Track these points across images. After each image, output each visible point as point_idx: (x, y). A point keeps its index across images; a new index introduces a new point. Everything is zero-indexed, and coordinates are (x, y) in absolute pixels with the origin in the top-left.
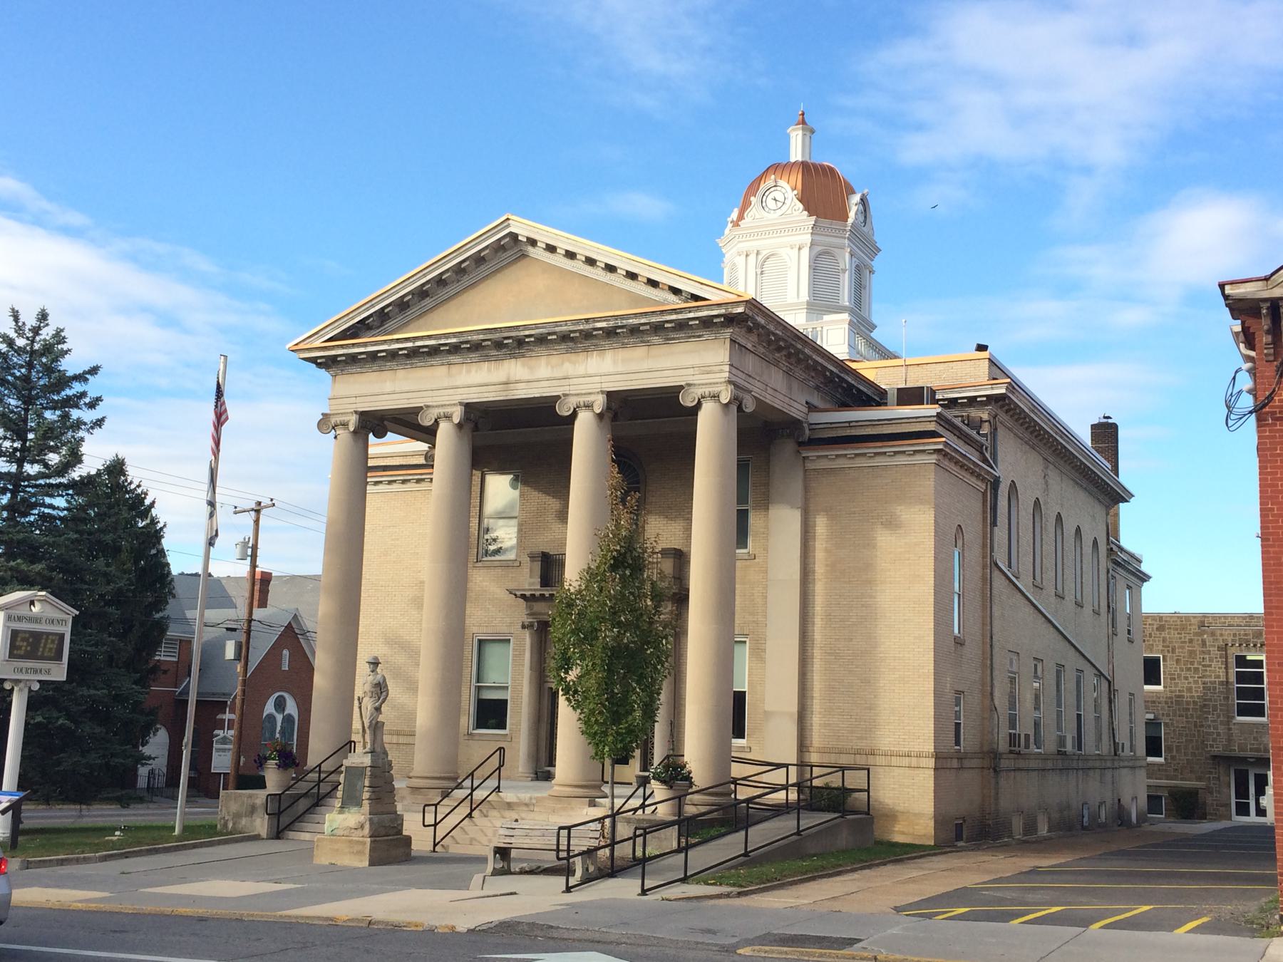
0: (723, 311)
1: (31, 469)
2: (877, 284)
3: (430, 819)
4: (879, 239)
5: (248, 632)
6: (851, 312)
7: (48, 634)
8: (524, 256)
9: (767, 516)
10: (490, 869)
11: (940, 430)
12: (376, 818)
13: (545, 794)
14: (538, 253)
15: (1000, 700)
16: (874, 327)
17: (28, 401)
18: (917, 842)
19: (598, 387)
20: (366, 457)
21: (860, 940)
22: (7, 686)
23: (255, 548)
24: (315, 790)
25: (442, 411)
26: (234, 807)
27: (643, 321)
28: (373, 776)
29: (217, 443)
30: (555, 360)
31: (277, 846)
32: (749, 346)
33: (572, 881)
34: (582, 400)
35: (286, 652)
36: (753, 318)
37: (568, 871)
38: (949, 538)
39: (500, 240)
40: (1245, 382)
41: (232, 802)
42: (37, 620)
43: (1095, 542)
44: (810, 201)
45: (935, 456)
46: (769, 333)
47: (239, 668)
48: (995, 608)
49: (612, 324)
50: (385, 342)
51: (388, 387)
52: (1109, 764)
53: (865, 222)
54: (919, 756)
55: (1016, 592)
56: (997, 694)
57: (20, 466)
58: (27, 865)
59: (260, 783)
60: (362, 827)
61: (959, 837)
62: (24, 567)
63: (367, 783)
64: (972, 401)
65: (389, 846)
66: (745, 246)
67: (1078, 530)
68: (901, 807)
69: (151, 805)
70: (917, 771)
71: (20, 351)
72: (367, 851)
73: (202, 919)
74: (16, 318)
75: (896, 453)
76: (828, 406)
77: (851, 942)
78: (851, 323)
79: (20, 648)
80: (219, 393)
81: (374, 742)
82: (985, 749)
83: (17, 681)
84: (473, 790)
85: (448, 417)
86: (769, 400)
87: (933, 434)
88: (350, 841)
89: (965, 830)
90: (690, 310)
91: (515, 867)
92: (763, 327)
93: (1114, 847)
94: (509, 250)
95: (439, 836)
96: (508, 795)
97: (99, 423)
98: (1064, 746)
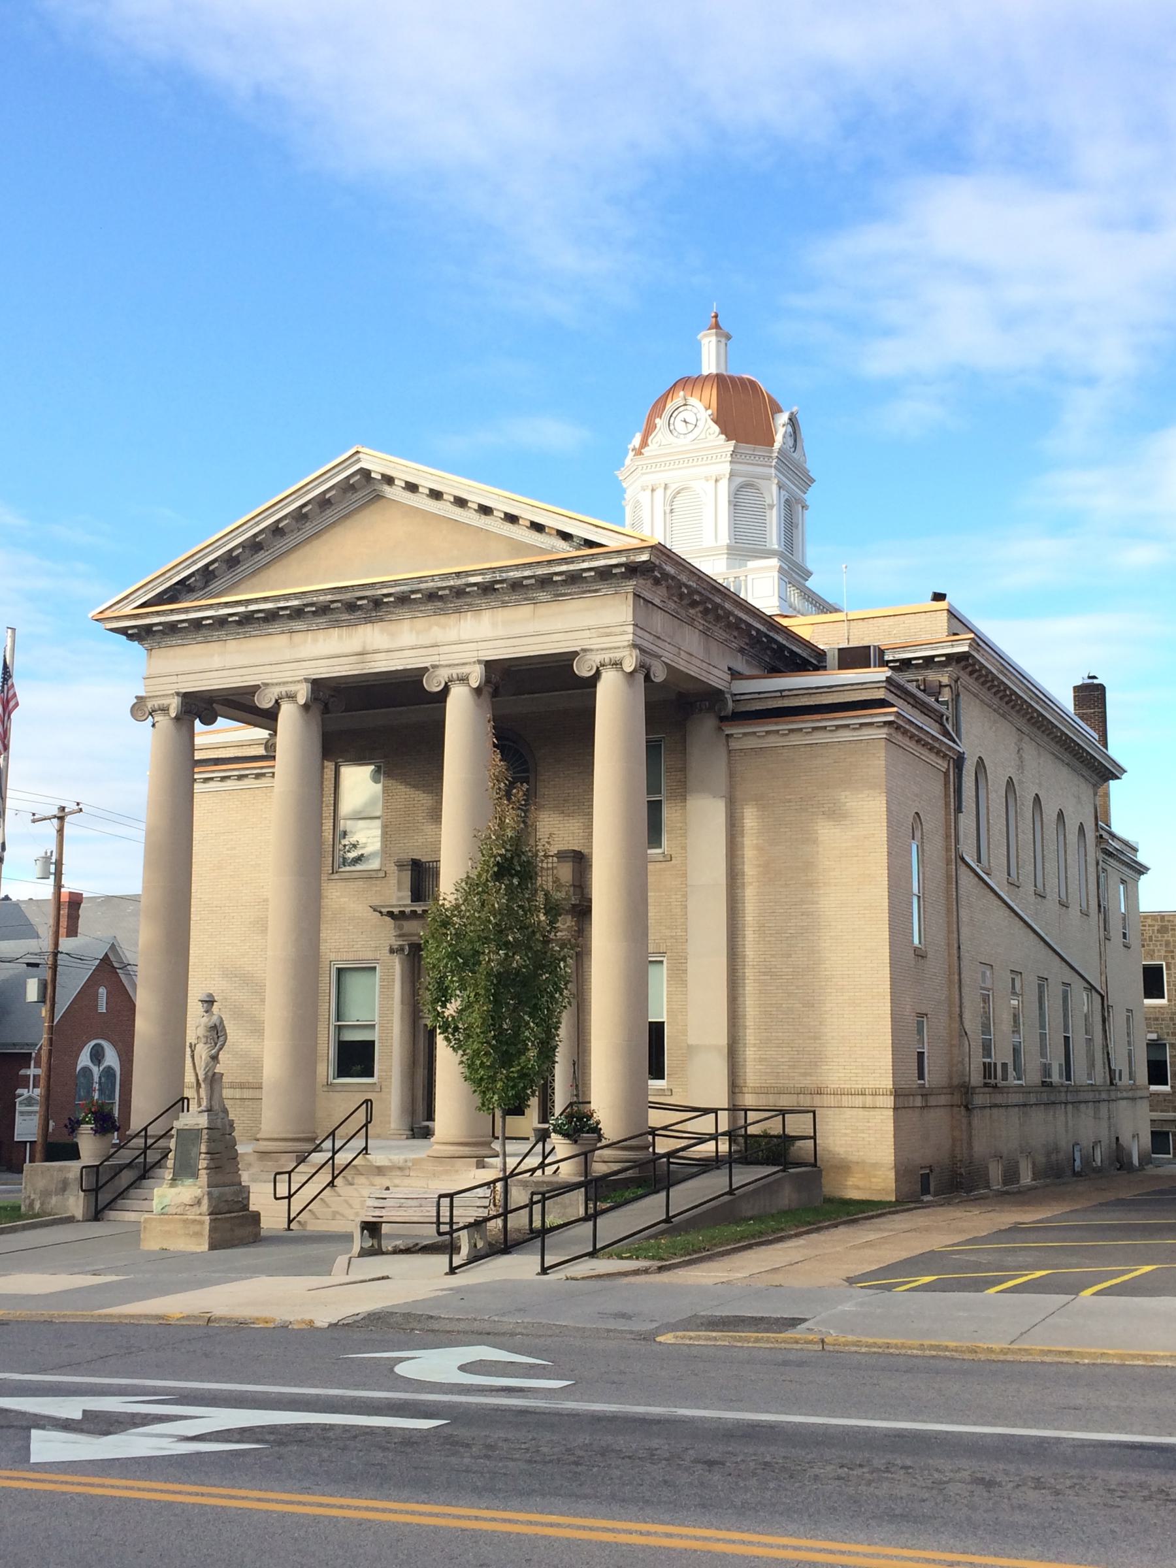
0: (623, 560)
2: (811, 521)
3: (283, 1190)
4: (813, 466)
5: (55, 968)
8: (379, 497)
10: (356, 1249)
11: (891, 698)
15: (972, 1024)
16: (809, 574)
18: (875, 1197)
19: (472, 656)
21: (805, 1320)
23: (59, 864)
24: (141, 1159)
26: (41, 1183)
27: (527, 573)
28: (210, 1140)
30: (420, 623)
31: (96, 1229)
32: (657, 601)
33: (457, 1260)
34: (455, 672)
35: (102, 991)
36: (660, 568)
37: (452, 1248)
38: (905, 828)
39: (348, 478)
43: (1081, 828)
44: (727, 422)
45: (885, 730)
46: (680, 584)
48: (962, 913)
49: (488, 578)
50: (211, 606)
51: (217, 662)
52: (1104, 1096)
53: (795, 446)
56: (967, 1016)
59: (73, 1153)
60: (199, 1202)
61: (925, 1190)
63: (203, 1149)
64: (929, 661)
65: (234, 1224)
67: (1061, 815)
68: (854, 1158)
76: (755, 672)
77: (794, 1322)
81: (210, 1099)
82: (956, 1082)
84: (334, 1153)
85: (291, 697)
86: (681, 665)
87: (882, 703)
88: (185, 1221)
89: (936, 1181)
90: (583, 558)
91: (387, 1245)
92: (673, 578)
93: (1111, 1196)
94: (360, 491)
96: (377, 1158)
98: (1050, 1076)
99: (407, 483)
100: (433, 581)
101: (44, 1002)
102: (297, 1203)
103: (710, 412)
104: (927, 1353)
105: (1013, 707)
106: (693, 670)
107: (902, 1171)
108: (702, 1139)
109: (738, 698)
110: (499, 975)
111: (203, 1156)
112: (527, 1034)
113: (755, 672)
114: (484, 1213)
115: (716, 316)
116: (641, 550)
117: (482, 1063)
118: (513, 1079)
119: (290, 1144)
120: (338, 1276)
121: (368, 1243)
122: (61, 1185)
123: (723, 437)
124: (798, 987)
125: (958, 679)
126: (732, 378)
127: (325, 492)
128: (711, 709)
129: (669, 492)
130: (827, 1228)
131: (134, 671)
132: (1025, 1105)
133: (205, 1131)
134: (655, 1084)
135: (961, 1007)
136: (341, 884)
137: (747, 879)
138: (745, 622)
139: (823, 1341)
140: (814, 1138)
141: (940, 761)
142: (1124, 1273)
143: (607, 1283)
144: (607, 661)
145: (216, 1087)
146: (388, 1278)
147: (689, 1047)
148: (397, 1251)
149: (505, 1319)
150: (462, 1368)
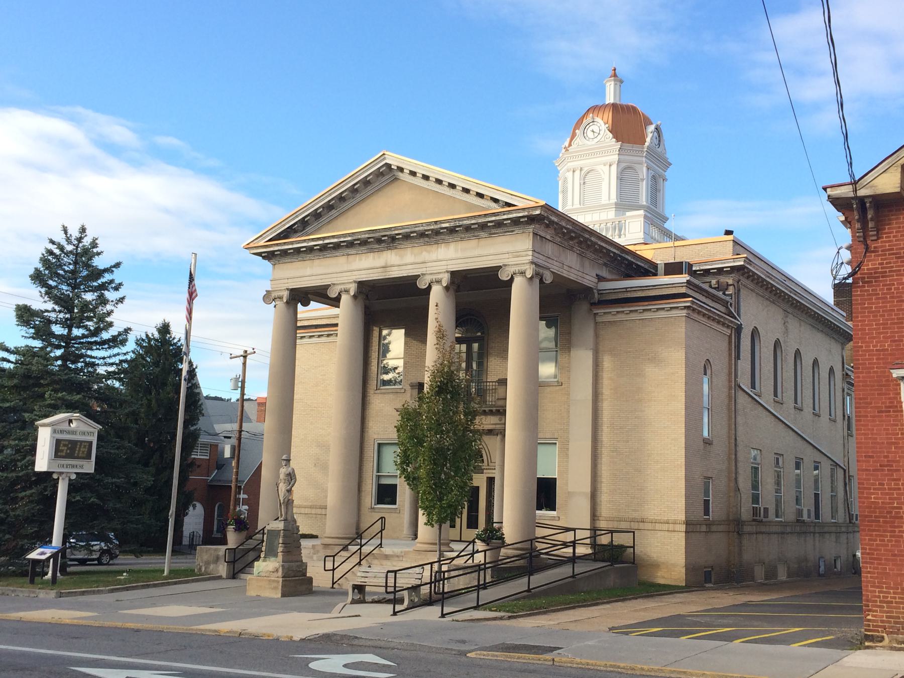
0: (526, 214)
1: (76, 332)
2: (670, 189)
3: (329, 565)
4: (670, 156)
5: (239, 439)
6: (647, 209)
7: (81, 442)
8: (396, 179)
9: (569, 355)
10: (350, 599)
11: (690, 292)
12: (286, 565)
15: (745, 483)
17: (75, 287)
18: (673, 583)
19: (444, 268)
20: (296, 320)
22: (55, 476)
23: (243, 382)
25: (343, 287)
26: (206, 557)
27: (473, 222)
28: (284, 536)
29: (190, 312)
30: (416, 250)
32: (548, 237)
34: (434, 277)
36: (548, 218)
38: (700, 368)
39: (379, 168)
40: (846, 255)
41: (205, 553)
42: (73, 432)
43: (831, 370)
44: (617, 132)
45: (685, 311)
46: (562, 227)
47: (234, 464)
48: (739, 419)
49: (452, 224)
50: (305, 241)
51: (308, 271)
52: (843, 529)
53: (659, 144)
54: (675, 523)
56: (741, 480)
57: (70, 331)
58: (60, 595)
59: (224, 541)
60: (277, 571)
62: (67, 397)
63: (281, 541)
64: (720, 271)
65: (297, 583)
66: (571, 165)
69: (189, 557)
70: (673, 534)
71: (67, 254)
72: (280, 587)
73: (138, 631)
74: (66, 231)
75: (658, 309)
76: (614, 277)
77: (552, 649)
78: (645, 217)
79: (62, 451)
80: (191, 279)
83: (61, 473)
84: (362, 546)
85: (347, 291)
87: (684, 295)
88: (269, 581)
89: (701, 577)
90: (504, 213)
91: (368, 598)
92: (557, 224)
94: (386, 175)
96: (386, 550)
97: (121, 300)
104: (609, 669)
107: (690, 568)
108: (565, 545)
113: (614, 277)
116: (535, 208)
120: (334, 613)
127: (366, 177)
130: (630, 599)
132: (783, 533)
134: (544, 514)
135: (736, 474)
137: (604, 397)
140: (633, 547)
141: (725, 329)
145: (290, 507)
148: (374, 602)
150: (345, 666)
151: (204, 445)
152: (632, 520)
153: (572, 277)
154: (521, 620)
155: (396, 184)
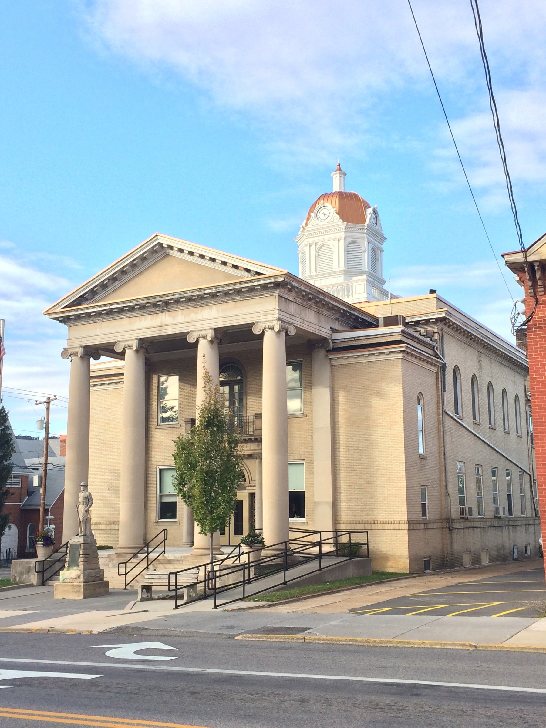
0: (272, 280)
2: (385, 258)
3: (122, 571)
4: (386, 232)
5: (46, 470)
6: (369, 274)
8: (168, 255)
10: (139, 597)
12: (87, 572)
13: (189, 554)
14: (174, 253)
15: (453, 490)
16: (384, 282)
19: (209, 326)
23: (47, 423)
25: (127, 343)
26: (19, 569)
27: (230, 288)
28: (84, 549)
30: (186, 312)
32: (291, 299)
34: (201, 333)
36: (290, 283)
39: (153, 247)
40: (522, 307)
43: (517, 397)
44: (343, 214)
45: (401, 354)
46: (302, 291)
47: (41, 491)
49: (214, 290)
51: (98, 331)
52: (531, 522)
54: (399, 523)
55: (461, 427)
56: (450, 486)
59: (34, 555)
60: (79, 577)
61: (427, 567)
63: (81, 553)
64: (427, 322)
65: (95, 587)
67: (504, 391)
68: (390, 553)
72: (82, 591)
77: (304, 630)
78: (368, 281)
81: (85, 530)
82: (444, 517)
84: (148, 554)
85: (130, 347)
86: (305, 328)
89: (423, 565)
90: (255, 280)
91: (155, 596)
92: (297, 288)
93: (520, 570)
94: (159, 252)
95: (129, 579)
96: (169, 556)
98: (499, 514)
99: (178, 249)
100: (190, 292)
101: (41, 486)
102: (130, 577)
103: (335, 209)
104: (349, 643)
105: (474, 341)
106: (312, 329)
107: (412, 559)
109: (335, 341)
110: (207, 473)
111: (81, 556)
112: (220, 498)
114: (195, 581)
115: (339, 165)
116: (280, 276)
117: (200, 512)
118: (214, 519)
119: (130, 550)
120: (127, 610)
121: (146, 595)
122: (27, 570)
123: (341, 220)
124: (364, 474)
125: (443, 329)
126: (346, 193)
127: (143, 254)
128: (322, 347)
129: (317, 246)
130: (366, 586)
131: (63, 336)
133: (82, 545)
134: (296, 521)
136: (160, 430)
138: (337, 306)
139: (304, 638)
140: (367, 544)
141: (433, 368)
142: (486, 605)
143: (239, 612)
144: (267, 327)
146: (147, 611)
147: (315, 503)
148: (158, 599)
149: (177, 629)
150: (135, 652)
151: (17, 477)
152: (366, 523)
153: (311, 330)
154: (279, 607)
155: (168, 259)
